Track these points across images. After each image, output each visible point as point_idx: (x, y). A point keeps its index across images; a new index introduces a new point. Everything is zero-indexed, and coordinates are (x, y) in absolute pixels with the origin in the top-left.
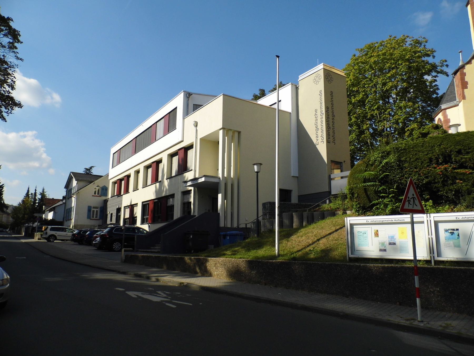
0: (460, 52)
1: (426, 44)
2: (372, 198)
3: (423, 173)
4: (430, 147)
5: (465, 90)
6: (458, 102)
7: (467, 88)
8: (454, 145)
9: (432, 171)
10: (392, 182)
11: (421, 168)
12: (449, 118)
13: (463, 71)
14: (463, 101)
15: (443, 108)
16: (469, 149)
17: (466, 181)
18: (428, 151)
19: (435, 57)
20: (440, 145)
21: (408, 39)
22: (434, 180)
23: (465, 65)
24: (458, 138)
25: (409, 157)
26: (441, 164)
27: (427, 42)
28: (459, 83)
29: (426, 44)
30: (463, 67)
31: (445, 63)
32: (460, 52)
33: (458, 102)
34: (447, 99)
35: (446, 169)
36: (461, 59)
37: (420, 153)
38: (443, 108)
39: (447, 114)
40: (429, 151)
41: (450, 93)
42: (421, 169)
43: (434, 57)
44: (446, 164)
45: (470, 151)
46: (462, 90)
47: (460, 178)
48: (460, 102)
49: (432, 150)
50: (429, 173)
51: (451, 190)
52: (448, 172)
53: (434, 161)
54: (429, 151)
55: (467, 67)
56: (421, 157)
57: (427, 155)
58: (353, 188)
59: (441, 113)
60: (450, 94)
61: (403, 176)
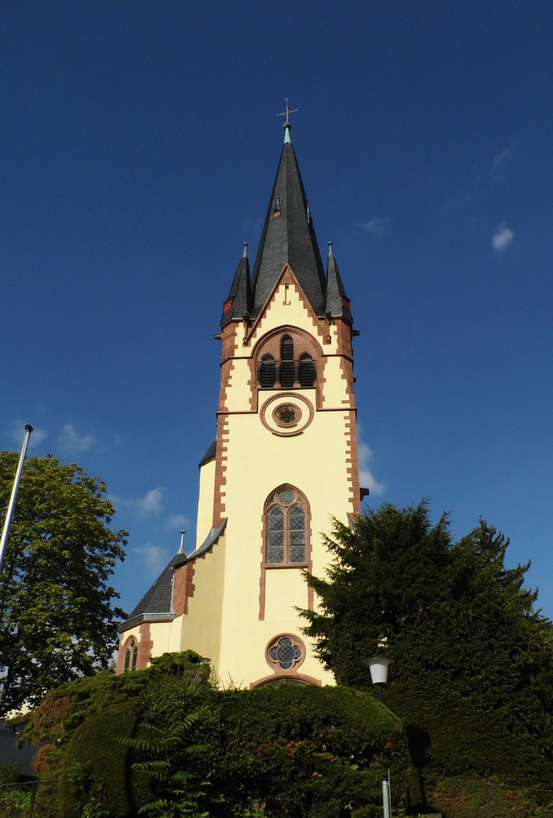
0: (182, 533)
1: (102, 493)
2: (139, 797)
3: (262, 752)
4: (283, 704)
5: (190, 598)
6: (173, 616)
7: (192, 596)
8: (322, 708)
9: (279, 749)
10: (198, 765)
11: (261, 741)
12: (151, 639)
13: (192, 567)
14: (184, 617)
15: (145, 619)
16: (342, 718)
17: (329, 775)
18: (257, 709)
19: (110, 522)
20: (299, 704)
21: (76, 474)
22: (279, 767)
23: (196, 558)
24: (328, 696)
25: (242, 717)
26: (293, 738)
27: (104, 491)
28: (181, 584)
29: (102, 493)
30: (193, 560)
31: (124, 538)
32: (182, 533)
33: (173, 616)
34: (154, 606)
35: (302, 750)
36: (182, 544)
37: (263, 713)
38: (145, 619)
39: (150, 631)
40: (279, 710)
41: (160, 596)
42: (259, 743)
43: (108, 520)
44: (302, 739)
45: (343, 722)
46: (186, 597)
47: (322, 768)
48: (176, 616)
49: (284, 710)
50: (272, 755)
51: (301, 791)
52: (305, 756)
53: (283, 732)
54: (279, 710)
55: (199, 561)
56: (263, 720)
57: (274, 717)
58: (93, 770)
59: (139, 627)
60: (159, 598)
61: (224, 754)
